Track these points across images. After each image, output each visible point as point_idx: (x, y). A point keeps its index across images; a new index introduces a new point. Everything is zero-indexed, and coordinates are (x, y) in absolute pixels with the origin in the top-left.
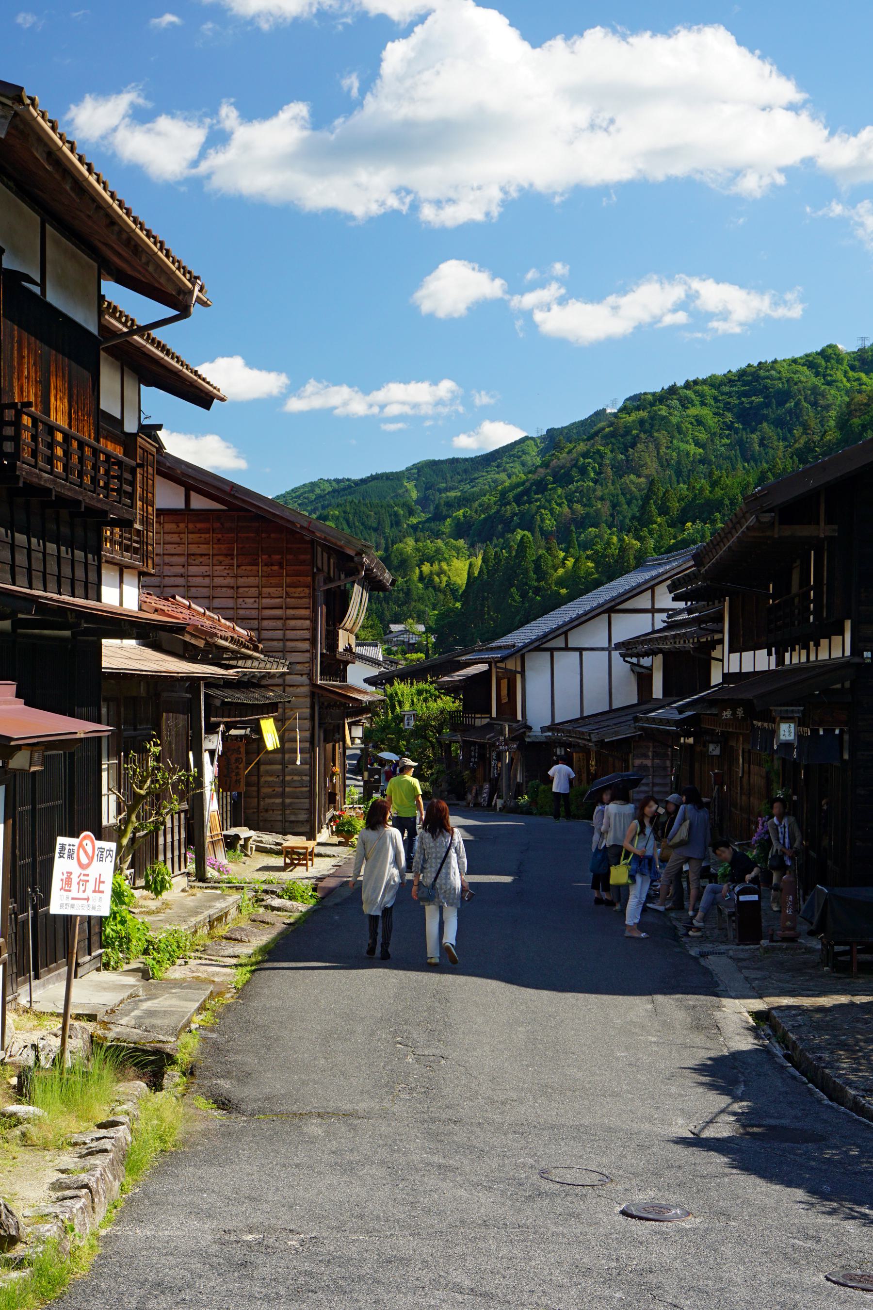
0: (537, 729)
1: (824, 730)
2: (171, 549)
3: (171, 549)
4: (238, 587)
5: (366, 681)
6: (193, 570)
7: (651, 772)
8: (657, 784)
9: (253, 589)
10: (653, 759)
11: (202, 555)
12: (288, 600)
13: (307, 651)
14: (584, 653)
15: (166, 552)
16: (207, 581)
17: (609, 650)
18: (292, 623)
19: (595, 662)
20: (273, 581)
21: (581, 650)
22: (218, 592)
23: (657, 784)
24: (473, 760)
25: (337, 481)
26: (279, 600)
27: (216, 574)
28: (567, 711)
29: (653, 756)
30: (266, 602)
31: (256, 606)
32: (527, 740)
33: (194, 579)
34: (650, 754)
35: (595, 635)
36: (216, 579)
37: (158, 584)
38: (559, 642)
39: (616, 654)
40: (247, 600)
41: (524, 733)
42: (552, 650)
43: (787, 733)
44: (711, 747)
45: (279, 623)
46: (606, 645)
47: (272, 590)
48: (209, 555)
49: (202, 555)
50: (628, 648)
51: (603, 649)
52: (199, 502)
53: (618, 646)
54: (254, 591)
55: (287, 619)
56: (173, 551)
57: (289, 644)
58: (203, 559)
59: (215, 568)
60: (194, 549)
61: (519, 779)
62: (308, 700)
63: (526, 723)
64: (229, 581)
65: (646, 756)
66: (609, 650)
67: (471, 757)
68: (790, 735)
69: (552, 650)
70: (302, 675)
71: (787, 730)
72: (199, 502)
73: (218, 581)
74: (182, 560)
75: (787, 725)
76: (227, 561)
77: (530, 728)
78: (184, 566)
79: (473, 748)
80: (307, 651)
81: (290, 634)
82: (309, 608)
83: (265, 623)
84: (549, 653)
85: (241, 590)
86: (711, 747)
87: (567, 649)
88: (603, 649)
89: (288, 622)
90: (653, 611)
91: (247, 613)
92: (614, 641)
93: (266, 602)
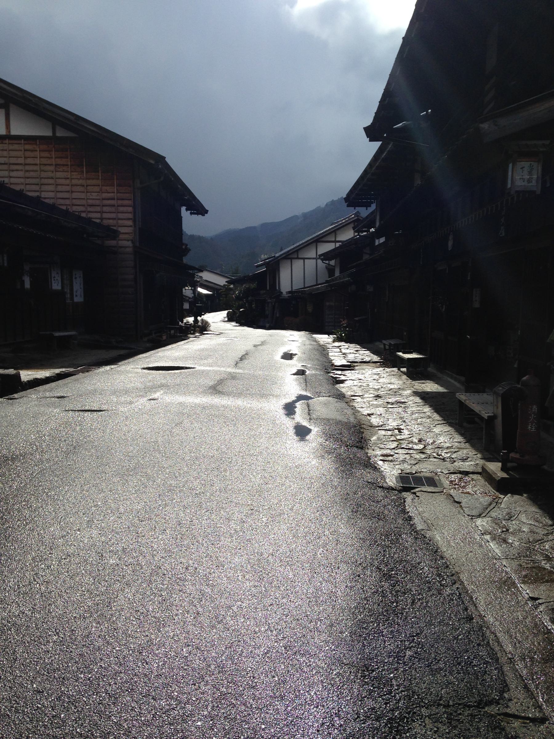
0: (284, 293)
2: (44, 161)
3: (44, 161)
4: (87, 186)
6: (59, 174)
9: (96, 187)
11: (64, 165)
12: (118, 194)
13: (131, 226)
15: (41, 163)
16: (68, 182)
17: (316, 259)
18: (121, 209)
21: (304, 259)
22: (75, 189)
26: (112, 194)
27: (73, 177)
30: (105, 195)
31: (98, 198)
33: (60, 180)
35: (312, 253)
36: (73, 181)
37: (37, 183)
39: (319, 261)
40: (93, 194)
42: (291, 259)
45: (113, 209)
46: (315, 257)
47: (108, 188)
48: (67, 165)
49: (64, 165)
50: (326, 257)
51: (314, 258)
52: (61, 133)
53: (320, 255)
54: (97, 189)
55: (118, 206)
56: (46, 162)
57: (120, 222)
58: (65, 168)
59: (73, 173)
61: (278, 315)
66: (316, 259)
70: (128, 240)
72: (61, 133)
73: (74, 182)
74: (52, 168)
78: (53, 172)
80: (131, 226)
81: (121, 216)
82: (131, 199)
83: (105, 209)
85: (89, 188)
87: (298, 258)
88: (314, 258)
89: (119, 208)
90: (335, 242)
91: (93, 202)
92: (318, 254)
93: (105, 195)
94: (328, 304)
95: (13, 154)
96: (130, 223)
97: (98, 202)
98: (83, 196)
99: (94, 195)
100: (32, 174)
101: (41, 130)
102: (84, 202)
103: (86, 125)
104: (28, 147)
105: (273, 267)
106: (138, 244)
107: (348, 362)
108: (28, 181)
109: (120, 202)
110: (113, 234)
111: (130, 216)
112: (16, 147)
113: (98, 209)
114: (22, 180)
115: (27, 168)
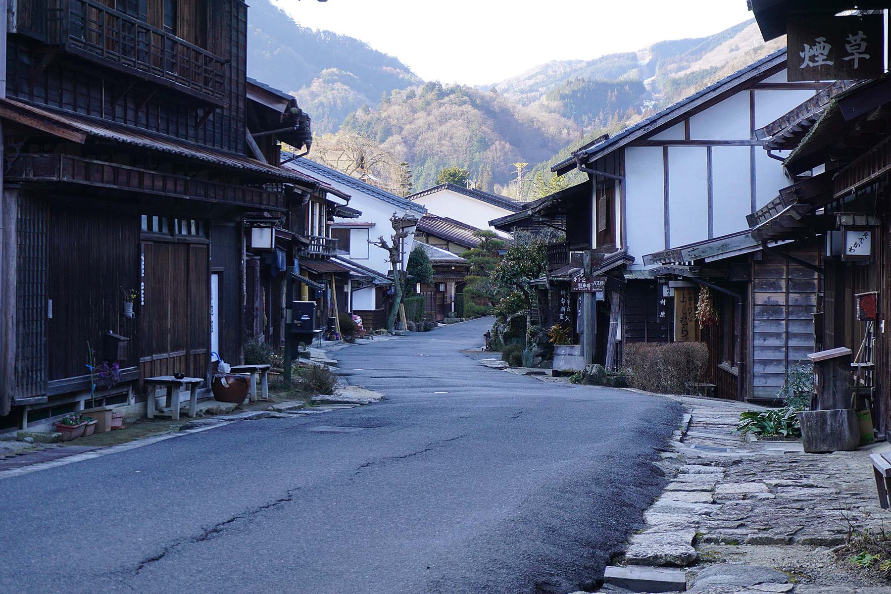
5: (491, 223)
7: (784, 316)
8: (795, 335)
10: (787, 293)
14: (713, 148)
19: (731, 163)
21: (709, 144)
23: (795, 335)
24: (563, 309)
25: (570, 63)
28: (688, 232)
29: (787, 287)
32: (627, 276)
34: (783, 283)
38: (677, 133)
39: (760, 151)
41: (624, 266)
42: (665, 144)
44: (852, 239)
51: (742, 143)
63: (625, 252)
65: (776, 287)
67: (561, 305)
69: (665, 144)
77: (632, 259)
79: (563, 293)
84: (661, 149)
87: (688, 142)
88: (742, 143)
107: (561, 170)
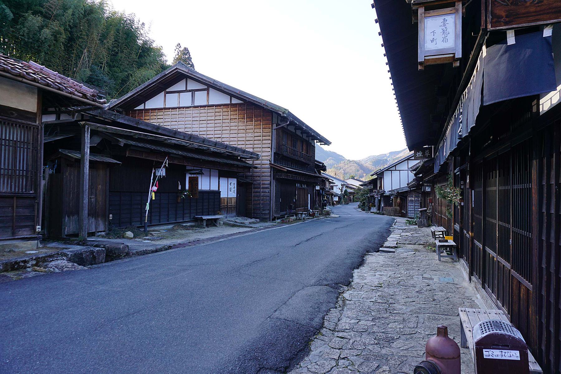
1: (518, 33)
6: (232, 124)
19: (404, 174)
20: (258, 127)
22: (240, 131)
28: (396, 187)
38: (394, 168)
43: (439, 36)
44: (427, 188)
45: (260, 142)
52: (235, 101)
60: (232, 117)
62: (269, 169)
64: (244, 127)
68: (445, 40)
71: (439, 31)
72: (235, 101)
74: (229, 121)
75: (440, 20)
76: (243, 120)
86: (427, 188)
94: (410, 199)
95: (209, 114)
96: (269, 150)
97: (251, 139)
98: (244, 135)
99: (250, 135)
100: (218, 125)
101: (225, 100)
102: (244, 139)
103: (432, 4)
104: (217, 110)
105: (380, 175)
106: (273, 163)
108: (216, 129)
109: (264, 138)
110: (255, 156)
111: (270, 146)
112: (211, 111)
113: (252, 142)
114: (213, 128)
115: (216, 121)
